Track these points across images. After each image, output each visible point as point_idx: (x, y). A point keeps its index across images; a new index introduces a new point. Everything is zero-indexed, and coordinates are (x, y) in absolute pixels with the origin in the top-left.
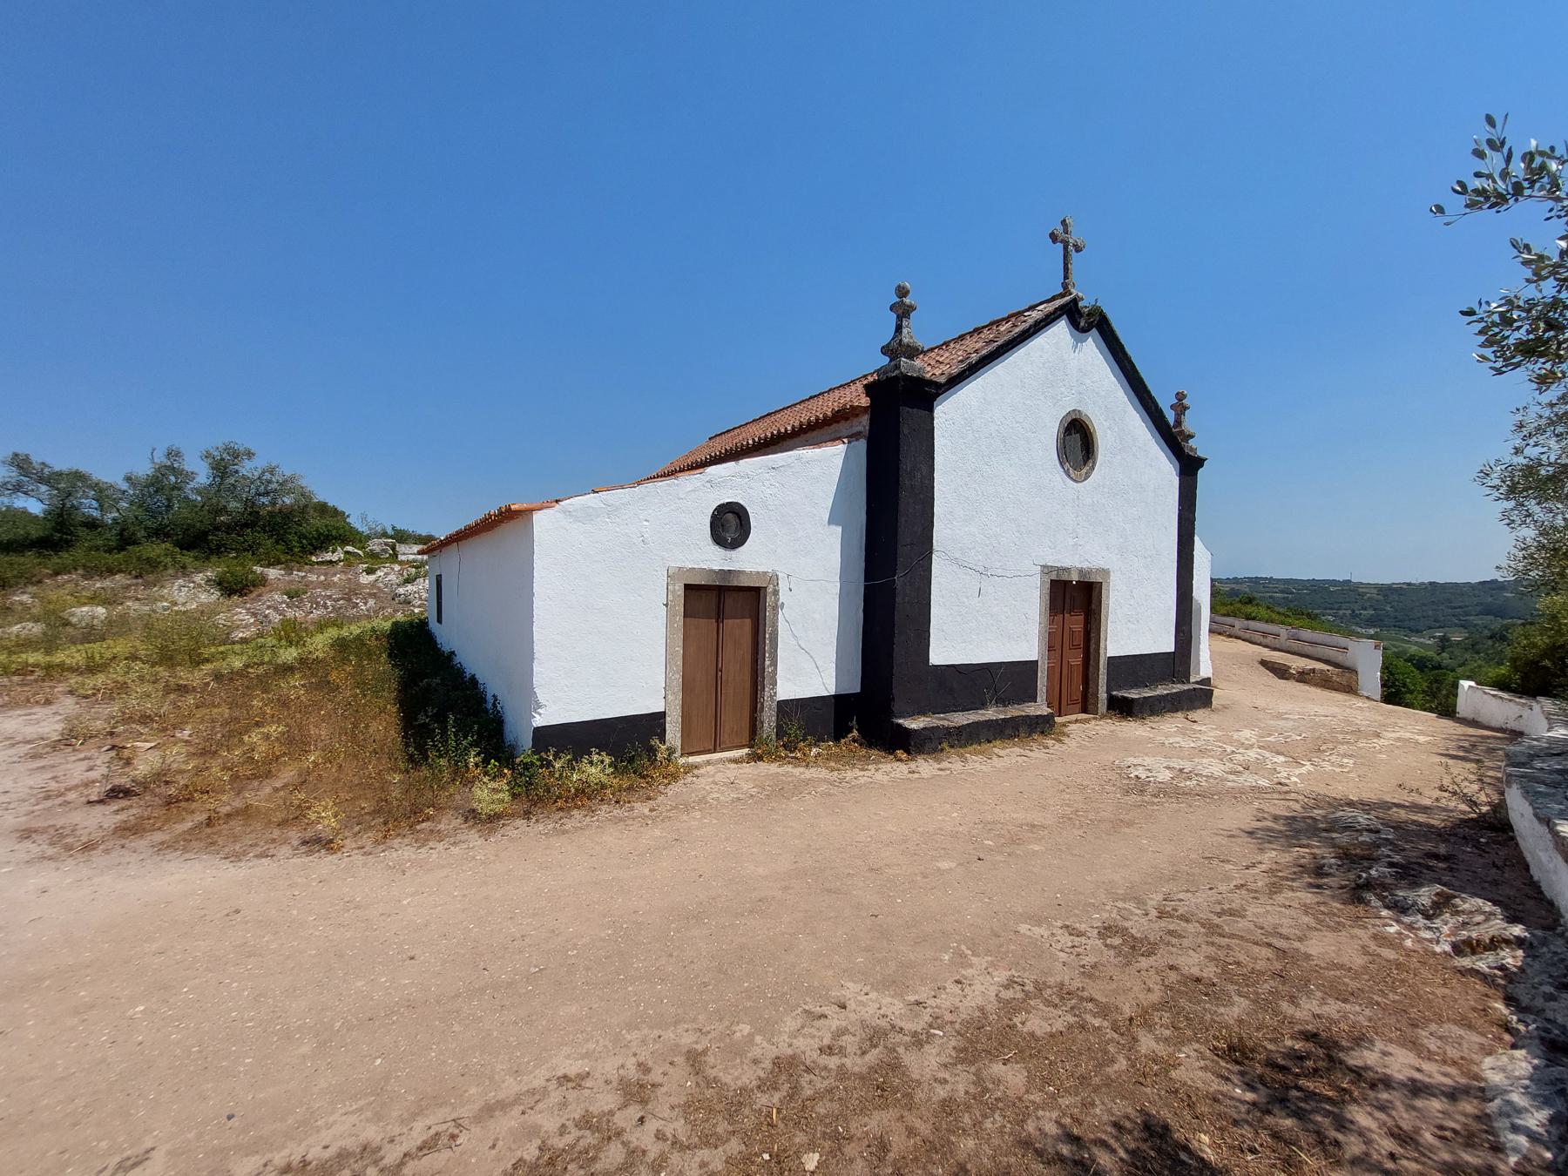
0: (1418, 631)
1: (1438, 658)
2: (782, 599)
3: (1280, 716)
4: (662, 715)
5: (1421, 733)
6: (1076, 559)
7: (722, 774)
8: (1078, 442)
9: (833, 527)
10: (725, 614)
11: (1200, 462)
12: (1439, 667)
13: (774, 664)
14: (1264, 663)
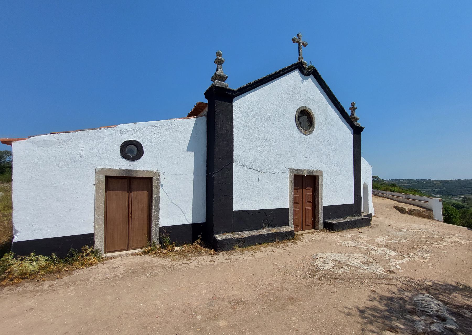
0: (455, 196)
1: (463, 204)
2: (162, 182)
3: (399, 230)
4: (93, 235)
5: (462, 239)
6: (306, 165)
7: (126, 260)
8: (305, 119)
9: (189, 153)
10: (128, 190)
11: (361, 129)
12: (463, 207)
13: (158, 210)
14: (396, 207)
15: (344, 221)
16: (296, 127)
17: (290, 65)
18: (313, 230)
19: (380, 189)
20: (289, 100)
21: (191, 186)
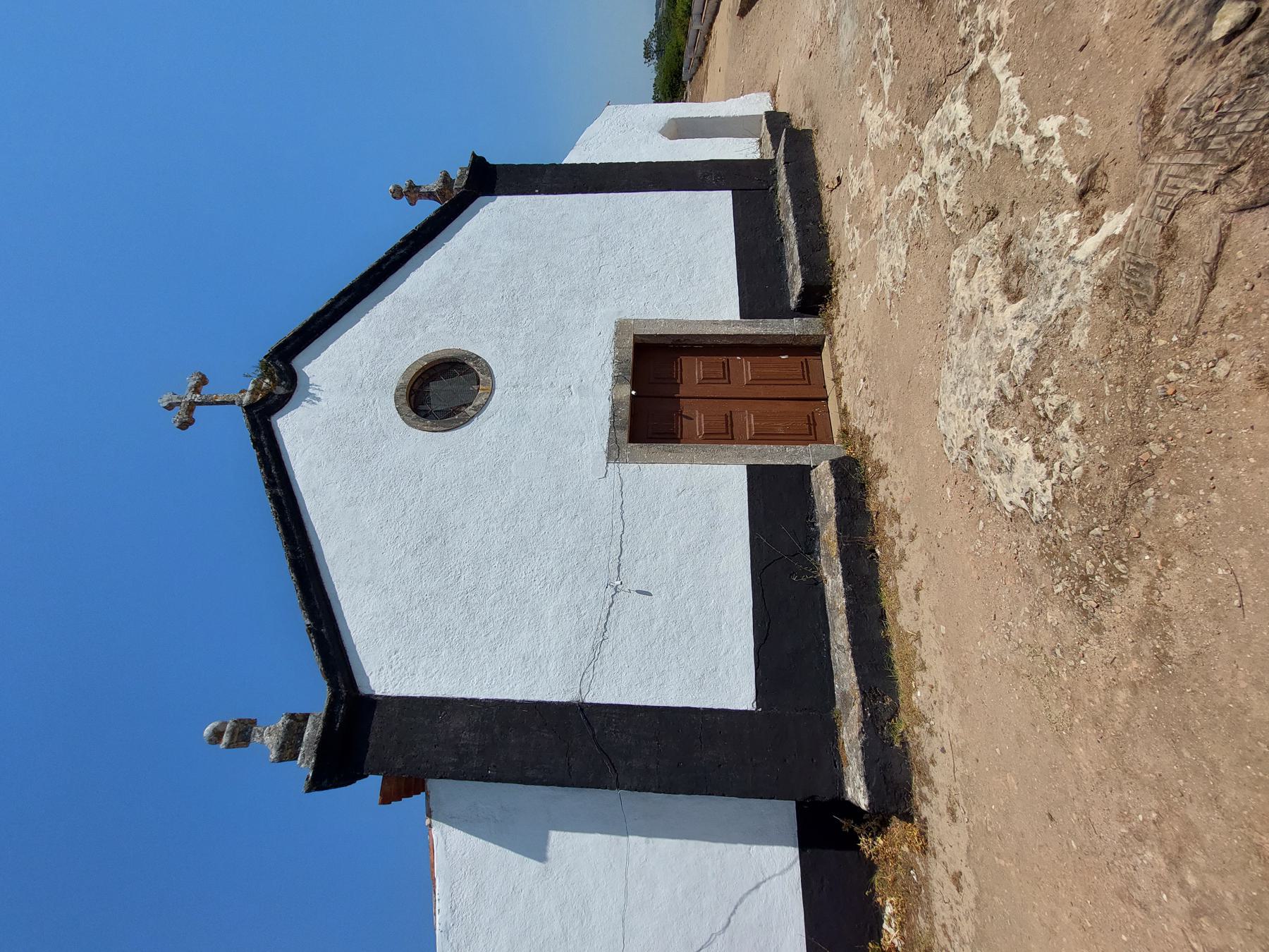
8: (441, 391)
9: (552, 851)
15: (793, 238)
16: (465, 429)
17: (255, 453)
18: (826, 353)
19: (684, 45)
20: (375, 456)
21: (666, 846)
